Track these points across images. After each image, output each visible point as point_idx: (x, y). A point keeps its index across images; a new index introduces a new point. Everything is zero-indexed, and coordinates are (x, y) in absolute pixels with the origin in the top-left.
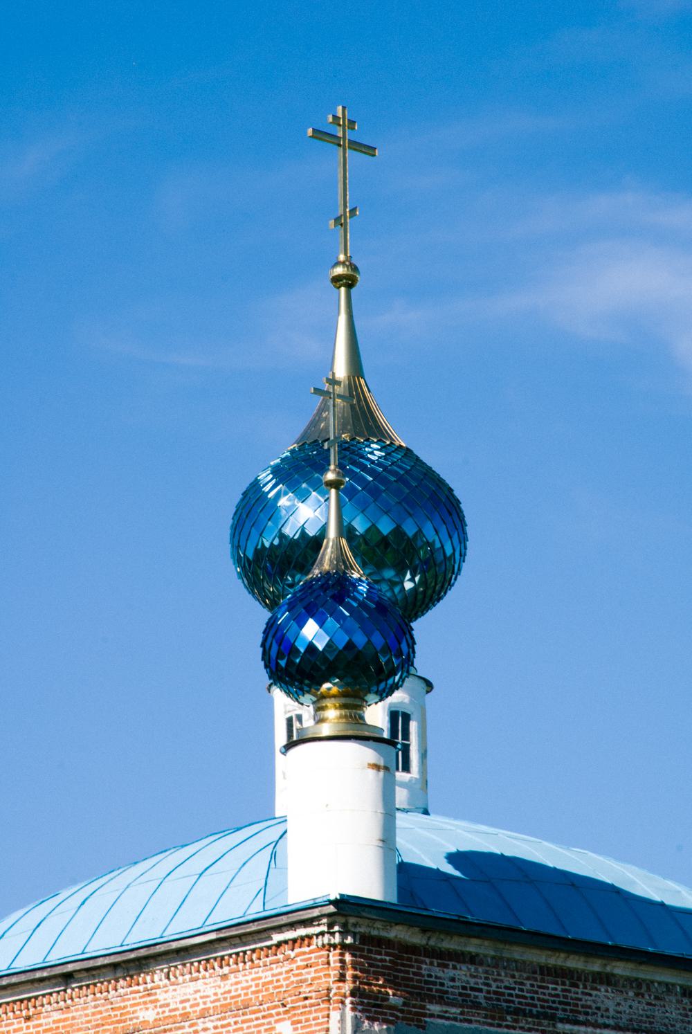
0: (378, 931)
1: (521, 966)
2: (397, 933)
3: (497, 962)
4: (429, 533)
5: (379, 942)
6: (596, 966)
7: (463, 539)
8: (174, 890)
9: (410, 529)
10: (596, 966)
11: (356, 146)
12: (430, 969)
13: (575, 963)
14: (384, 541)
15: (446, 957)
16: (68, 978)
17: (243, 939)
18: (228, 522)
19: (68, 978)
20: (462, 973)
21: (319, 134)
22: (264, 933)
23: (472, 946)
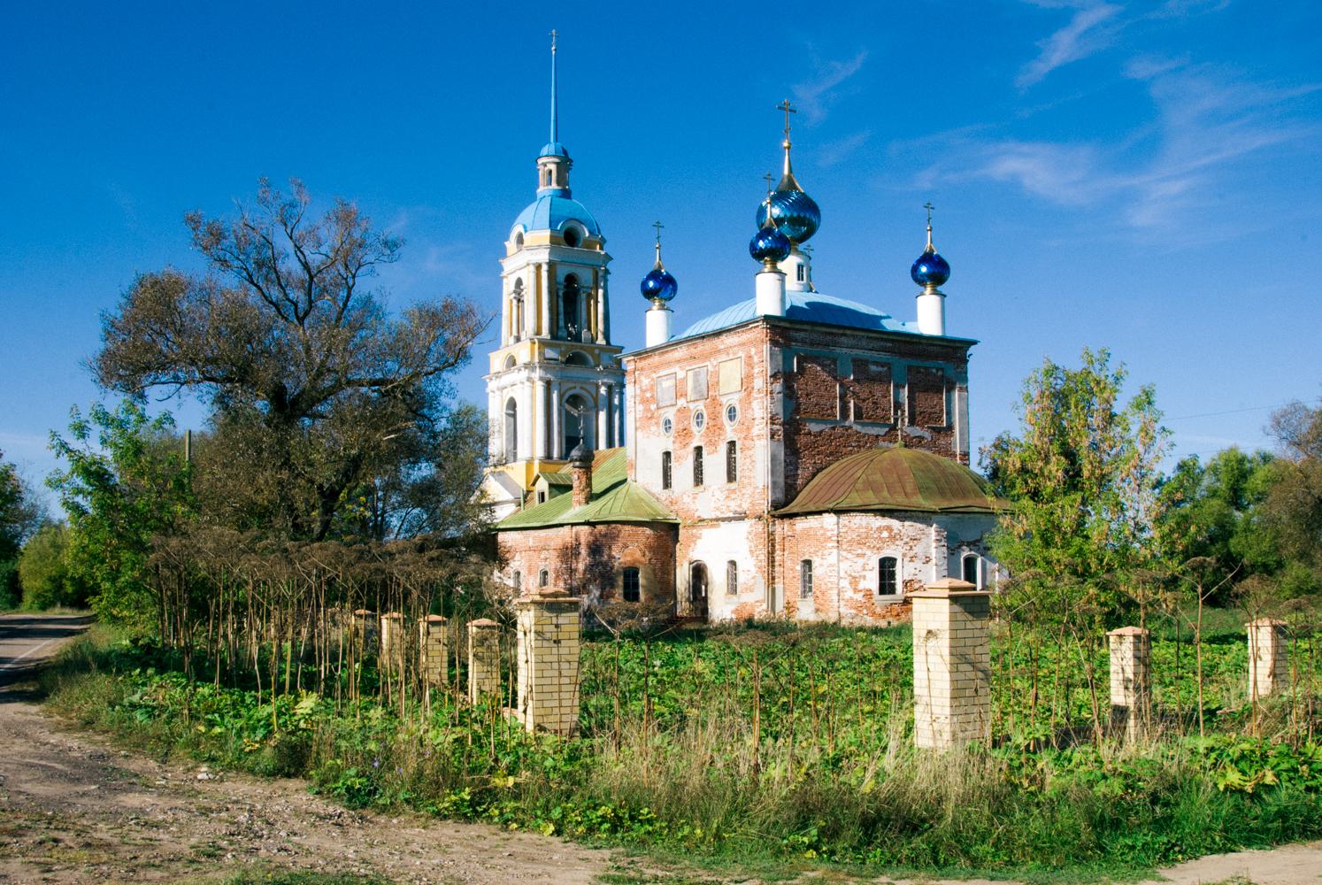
0: (777, 323)
1: (819, 332)
2: (782, 324)
3: (812, 331)
4: (808, 216)
5: (777, 327)
6: (841, 332)
7: (819, 217)
8: (742, 313)
9: (802, 215)
10: (841, 332)
11: (791, 111)
12: (793, 334)
13: (835, 331)
14: (794, 219)
15: (797, 330)
16: (703, 337)
17: (742, 326)
18: (755, 214)
19: (703, 337)
20: (802, 334)
21: (779, 108)
22: (747, 325)
23: (805, 327)
